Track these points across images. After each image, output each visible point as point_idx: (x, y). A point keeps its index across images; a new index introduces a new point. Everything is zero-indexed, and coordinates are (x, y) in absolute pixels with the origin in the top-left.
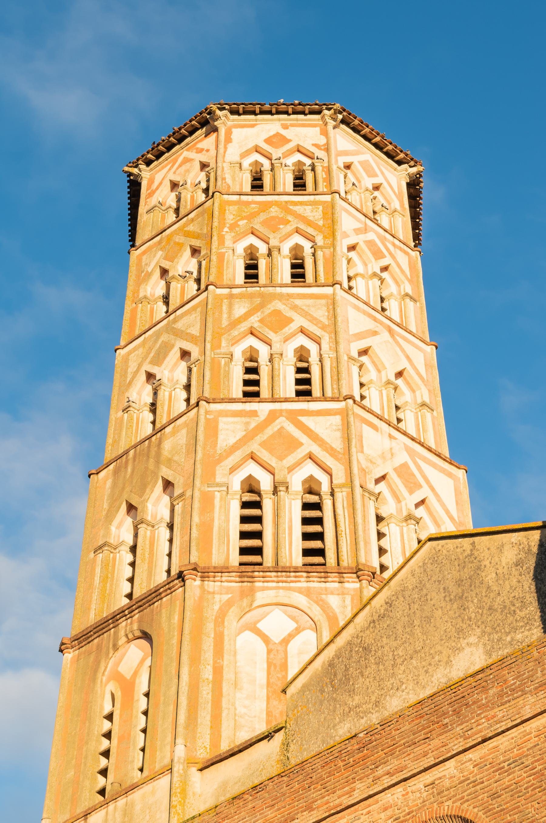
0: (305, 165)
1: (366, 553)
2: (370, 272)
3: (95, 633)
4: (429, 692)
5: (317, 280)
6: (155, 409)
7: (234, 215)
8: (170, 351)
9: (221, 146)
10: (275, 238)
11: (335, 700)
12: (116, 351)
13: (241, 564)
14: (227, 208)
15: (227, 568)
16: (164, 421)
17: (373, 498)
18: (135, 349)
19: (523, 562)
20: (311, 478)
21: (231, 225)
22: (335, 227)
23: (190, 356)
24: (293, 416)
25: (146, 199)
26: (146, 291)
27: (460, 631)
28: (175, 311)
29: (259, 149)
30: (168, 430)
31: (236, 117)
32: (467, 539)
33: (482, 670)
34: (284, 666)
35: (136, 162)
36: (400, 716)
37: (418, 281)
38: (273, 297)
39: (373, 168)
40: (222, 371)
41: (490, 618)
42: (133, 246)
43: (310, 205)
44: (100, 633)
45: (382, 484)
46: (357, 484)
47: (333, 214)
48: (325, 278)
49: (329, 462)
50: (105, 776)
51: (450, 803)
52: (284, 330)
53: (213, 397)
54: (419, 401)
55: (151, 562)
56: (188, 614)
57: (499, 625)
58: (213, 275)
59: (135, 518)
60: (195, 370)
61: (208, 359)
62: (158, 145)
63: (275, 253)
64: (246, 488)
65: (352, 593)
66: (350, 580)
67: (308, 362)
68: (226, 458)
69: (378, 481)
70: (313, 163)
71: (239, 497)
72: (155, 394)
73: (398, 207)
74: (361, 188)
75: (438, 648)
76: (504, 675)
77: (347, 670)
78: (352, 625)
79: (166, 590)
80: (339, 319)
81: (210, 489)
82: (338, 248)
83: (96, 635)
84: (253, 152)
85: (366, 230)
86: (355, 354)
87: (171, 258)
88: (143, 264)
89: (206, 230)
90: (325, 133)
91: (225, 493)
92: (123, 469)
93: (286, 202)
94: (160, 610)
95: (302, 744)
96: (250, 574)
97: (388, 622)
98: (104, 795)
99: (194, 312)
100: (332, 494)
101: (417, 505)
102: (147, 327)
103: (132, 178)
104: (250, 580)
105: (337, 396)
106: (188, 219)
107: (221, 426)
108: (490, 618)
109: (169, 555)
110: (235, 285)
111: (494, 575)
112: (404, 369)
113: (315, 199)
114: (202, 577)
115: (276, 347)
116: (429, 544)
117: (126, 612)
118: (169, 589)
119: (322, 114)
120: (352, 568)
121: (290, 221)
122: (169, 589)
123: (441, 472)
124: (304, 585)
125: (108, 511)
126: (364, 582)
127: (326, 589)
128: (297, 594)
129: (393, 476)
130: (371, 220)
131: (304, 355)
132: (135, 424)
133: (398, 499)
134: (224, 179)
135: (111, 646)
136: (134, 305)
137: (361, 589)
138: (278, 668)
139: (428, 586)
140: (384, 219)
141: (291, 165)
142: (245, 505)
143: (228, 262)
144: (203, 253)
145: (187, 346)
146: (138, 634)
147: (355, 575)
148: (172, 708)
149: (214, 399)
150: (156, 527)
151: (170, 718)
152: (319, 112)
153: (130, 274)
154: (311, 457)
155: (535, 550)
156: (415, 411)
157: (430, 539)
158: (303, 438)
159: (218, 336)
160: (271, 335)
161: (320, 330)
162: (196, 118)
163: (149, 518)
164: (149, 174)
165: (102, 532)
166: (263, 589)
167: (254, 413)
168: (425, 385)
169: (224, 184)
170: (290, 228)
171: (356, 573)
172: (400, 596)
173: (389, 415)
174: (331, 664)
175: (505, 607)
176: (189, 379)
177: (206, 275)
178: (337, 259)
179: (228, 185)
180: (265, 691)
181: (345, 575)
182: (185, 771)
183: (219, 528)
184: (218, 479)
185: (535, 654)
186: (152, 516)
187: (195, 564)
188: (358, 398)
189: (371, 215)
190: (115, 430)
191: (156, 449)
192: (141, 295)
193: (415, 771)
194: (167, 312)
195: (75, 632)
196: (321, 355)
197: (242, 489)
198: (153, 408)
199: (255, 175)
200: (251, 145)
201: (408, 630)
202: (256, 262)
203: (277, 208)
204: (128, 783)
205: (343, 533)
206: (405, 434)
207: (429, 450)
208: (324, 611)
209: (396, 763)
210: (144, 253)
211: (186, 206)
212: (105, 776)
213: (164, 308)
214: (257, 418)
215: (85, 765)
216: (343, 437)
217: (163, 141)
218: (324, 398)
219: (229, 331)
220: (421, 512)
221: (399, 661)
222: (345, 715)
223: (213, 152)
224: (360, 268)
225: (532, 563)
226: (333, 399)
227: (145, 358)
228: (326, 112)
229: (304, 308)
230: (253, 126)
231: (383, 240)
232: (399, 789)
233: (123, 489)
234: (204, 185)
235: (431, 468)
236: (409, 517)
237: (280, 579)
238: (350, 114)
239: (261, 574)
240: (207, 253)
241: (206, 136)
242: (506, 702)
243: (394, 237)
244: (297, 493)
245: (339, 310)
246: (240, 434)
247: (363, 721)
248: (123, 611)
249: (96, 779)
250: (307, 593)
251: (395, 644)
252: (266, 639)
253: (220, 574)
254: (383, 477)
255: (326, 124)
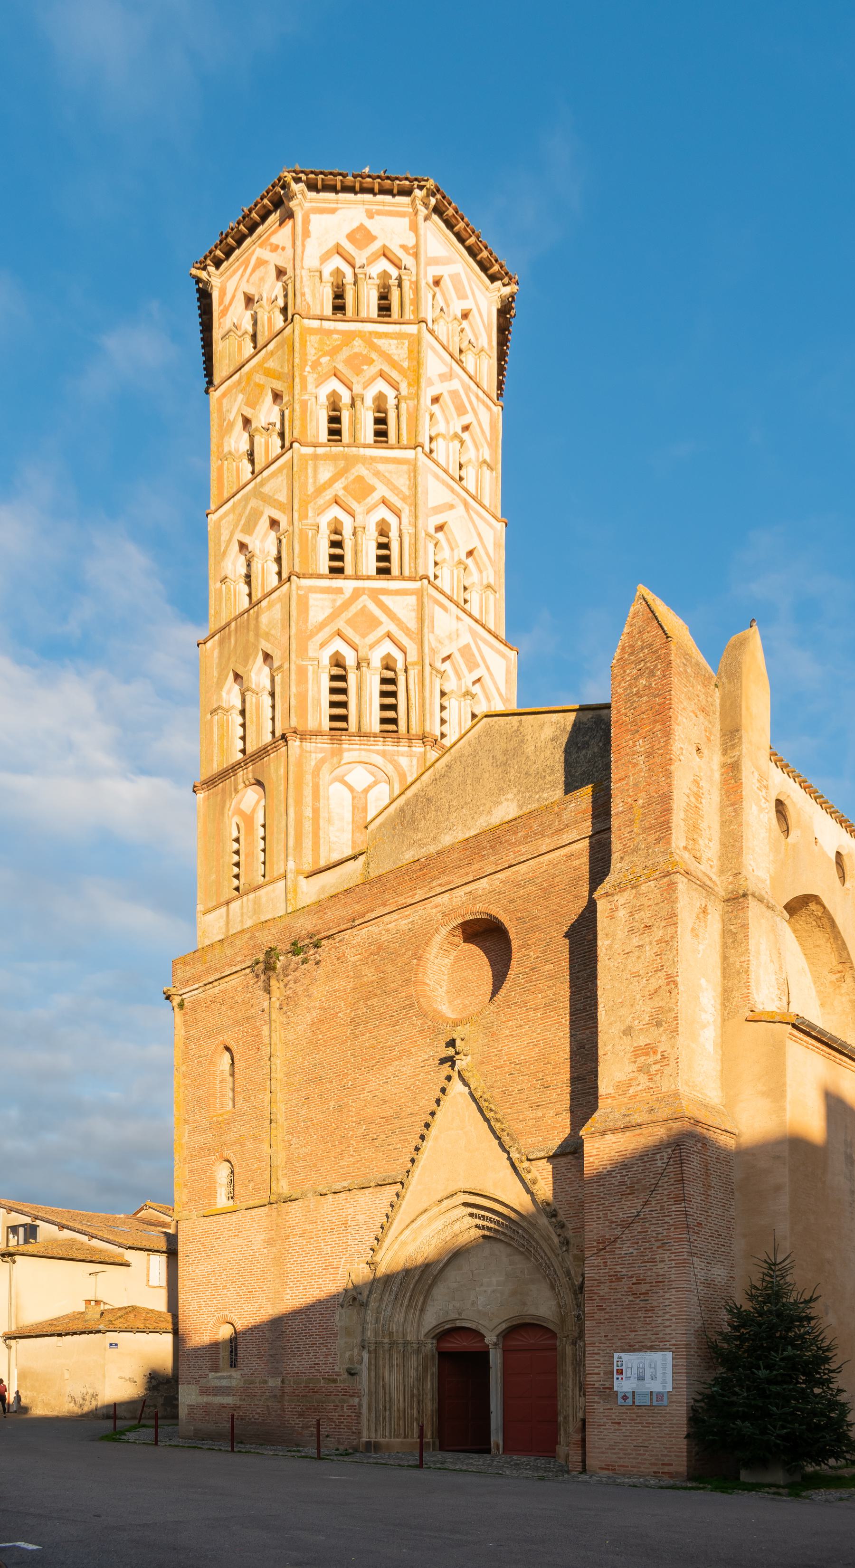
0: (390, 277)
1: (431, 723)
2: (452, 432)
3: (219, 779)
4: (473, 833)
5: (400, 441)
6: (250, 581)
7: (315, 348)
8: (260, 519)
9: (299, 243)
10: (358, 383)
11: (404, 835)
12: (207, 516)
13: (331, 729)
14: (308, 338)
15: (321, 732)
16: (259, 595)
17: (439, 676)
18: (226, 514)
19: (557, 738)
20: (389, 655)
21: (313, 362)
22: (421, 371)
23: (279, 526)
24: (374, 595)
25: (219, 320)
26: (230, 445)
27: (501, 789)
28: (262, 473)
29: (341, 251)
30: (264, 603)
31: (313, 195)
32: (516, 717)
33: (515, 819)
34: (365, 809)
35: (204, 262)
36: (452, 848)
37: (497, 445)
38: (358, 459)
39: (464, 287)
40: (310, 544)
41: (525, 781)
42: (210, 383)
43: (396, 338)
44: (223, 779)
45: (448, 662)
46: (427, 662)
47: (419, 352)
48: (407, 439)
49: (405, 641)
50: (238, 879)
51: (481, 904)
52: (367, 501)
53: (304, 572)
54: (485, 582)
55: (258, 725)
56: (291, 768)
57: (531, 786)
58: (297, 428)
59: (241, 685)
60: (284, 541)
61: (296, 531)
62: (227, 236)
63: (358, 403)
64: (334, 662)
65: (418, 755)
66: (417, 745)
67: (388, 537)
68: (317, 634)
69: (444, 660)
70: (400, 276)
71: (328, 671)
72: (249, 565)
73: (486, 346)
74: (449, 316)
75: (483, 801)
76: (531, 823)
77: (413, 814)
78: (419, 782)
79: (272, 748)
80: (420, 489)
81: (304, 663)
82: (422, 401)
83: (220, 781)
84: (333, 255)
85: (451, 376)
86: (432, 530)
87: (253, 404)
88: (224, 410)
89: (286, 368)
90: (414, 228)
91: (316, 667)
92: (227, 640)
93: (370, 333)
94: (269, 764)
95: (378, 864)
96: (338, 737)
97: (447, 781)
98: (239, 892)
99: (280, 475)
100: (406, 671)
101: (474, 683)
102: (235, 490)
103: (201, 285)
104: (339, 742)
105: (414, 575)
106: (267, 351)
107: (311, 602)
108: (525, 781)
109: (273, 719)
110: (318, 443)
111: (533, 747)
112: (475, 548)
113: (400, 330)
114: (300, 739)
115: (360, 518)
116: (485, 719)
117: (242, 764)
118: (275, 747)
119: (413, 195)
120: (419, 736)
121: (373, 361)
122: (275, 747)
123: (496, 652)
124: (381, 748)
125: (218, 678)
126: (428, 747)
127: (398, 751)
128: (375, 755)
129: (457, 656)
130: (457, 363)
131: (385, 529)
132: (233, 596)
133: (459, 677)
134: (303, 295)
135: (233, 789)
136: (220, 462)
137: (425, 753)
138: (360, 811)
139: (480, 753)
140: (469, 360)
141: (375, 277)
142: (334, 678)
143: (311, 412)
144: (286, 399)
145: (277, 515)
146: (253, 781)
147: (421, 741)
148: (283, 836)
149: (304, 574)
150: (260, 695)
151: (283, 843)
152: (407, 192)
153: (212, 423)
154: (389, 635)
155: (569, 728)
156: (480, 592)
157: (486, 716)
158: (383, 617)
159: (305, 504)
160: (354, 505)
161: (401, 502)
162: (268, 193)
163: (253, 686)
164: (219, 281)
165: (215, 697)
166: (349, 750)
167: (340, 591)
168: (492, 566)
169: (304, 303)
170: (373, 370)
171: (422, 740)
172: (458, 761)
173: (458, 597)
174: (402, 810)
175: (538, 773)
176: (279, 552)
177: (289, 429)
178: (421, 414)
179: (308, 304)
180: (350, 826)
181: (413, 741)
182: (296, 878)
183: (313, 698)
184: (311, 654)
185: (556, 809)
186: (256, 685)
187: (295, 728)
188: (432, 578)
189: (456, 354)
190: (215, 600)
191: (254, 622)
192: (226, 450)
193: (459, 884)
194: (253, 472)
195: (203, 778)
196: (400, 530)
197: (330, 663)
198: (248, 578)
199: (336, 289)
200: (331, 244)
201: (462, 787)
202: (338, 413)
203: (360, 341)
204: (255, 884)
205: (413, 706)
206: (470, 615)
207: (489, 631)
208: (396, 768)
209: (446, 879)
210: (224, 395)
211: (263, 332)
212: (238, 879)
213: (249, 468)
214: (342, 596)
215: (223, 871)
216: (418, 618)
217: (232, 229)
218: (402, 577)
219: (315, 498)
220: (476, 689)
221: (453, 809)
222: (410, 846)
223: (289, 252)
224: (441, 427)
225: (565, 739)
226: (411, 579)
227: (236, 526)
228: (417, 192)
229: (387, 474)
230: (333, 211)
231: (467, 389)
232: (447, 895)
233: (229, 659)
234: (281, 303)
235: (489, 650)
236: (467, 693)
237: (362, 742)
238: (444, 197)
239: (347, 737)
240: (289, 400)
241: (280, 225)
242: (529, 842)
243: (478, 386)
244: (376, 669)
245: (420, 479)
246: (328, 611)
247: (423, 850)
248: (240, 764)
249: (232, 881)
250: (383, 754)
251: (450, 797)
252: (351, 789)
253: (315, 737)
254: (449, 657)
255: (416, 213)
